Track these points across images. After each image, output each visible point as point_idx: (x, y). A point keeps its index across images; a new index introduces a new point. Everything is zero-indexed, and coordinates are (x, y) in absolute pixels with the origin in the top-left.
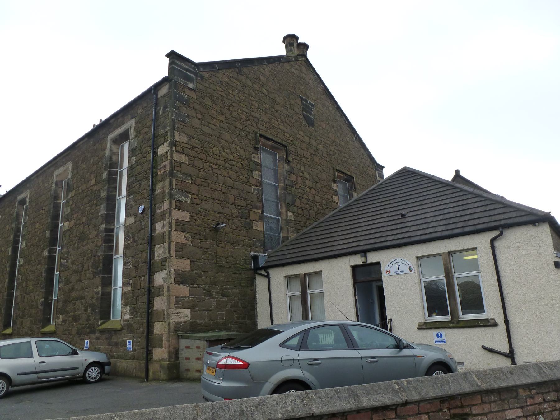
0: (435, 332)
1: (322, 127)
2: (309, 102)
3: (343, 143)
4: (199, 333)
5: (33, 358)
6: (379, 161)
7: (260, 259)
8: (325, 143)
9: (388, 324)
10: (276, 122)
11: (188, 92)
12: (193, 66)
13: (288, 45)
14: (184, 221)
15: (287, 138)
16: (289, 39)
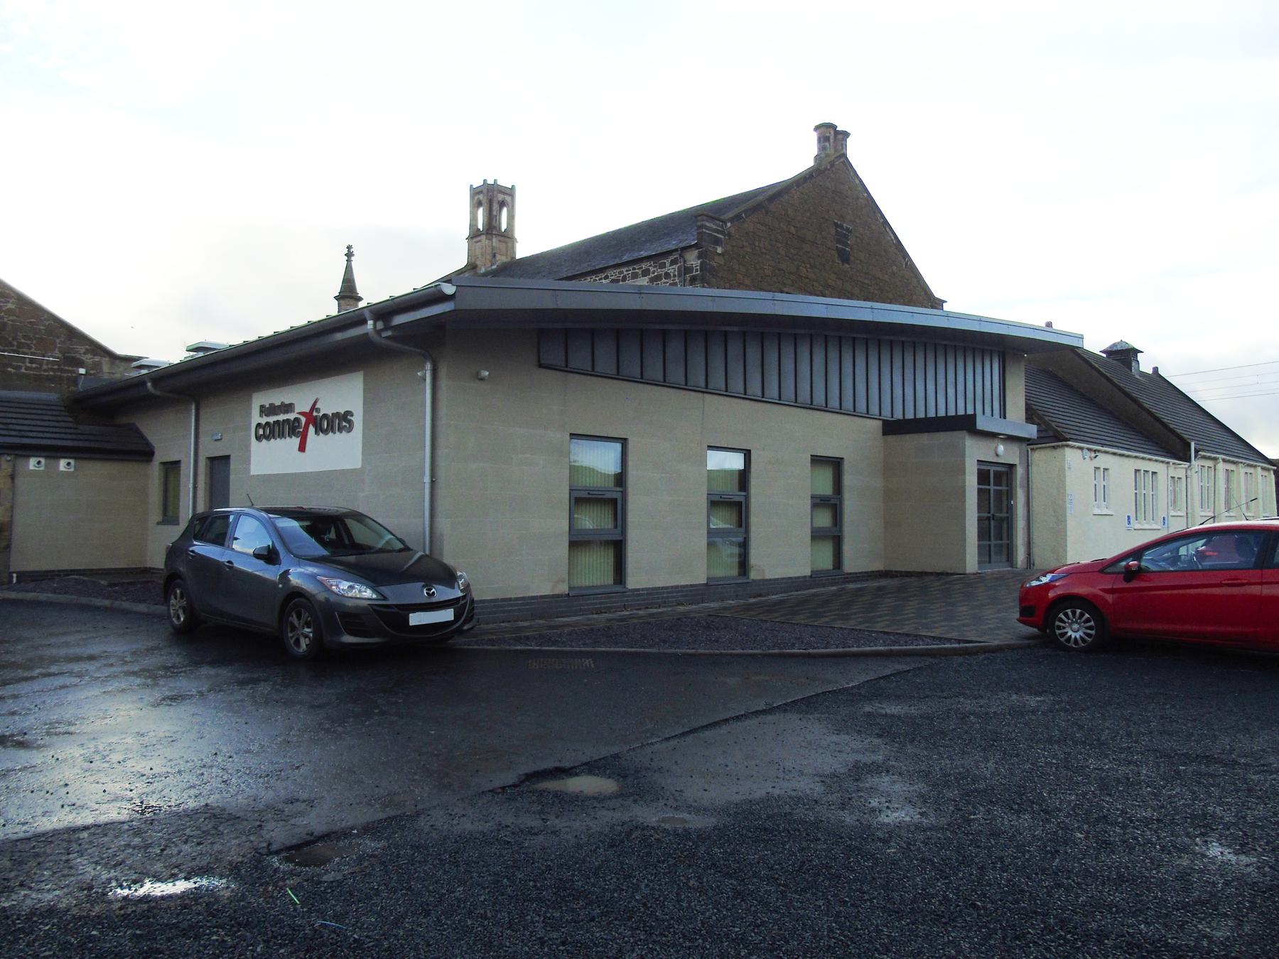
0: (434, 600)
1: (860, 260)
2: (847, 227)
3: (886, 278)
4: (1012, 521)
5: (814, 526)
6: (937, 295)
7: (845, 463)
8: (863, 283)
9: (42, 443)
10: (804, 270)
11: (717, 258)
12: (721, 223)
13: (822, 140)
14: (1162, 574)
15: (816, 288)
16: (823, 129)
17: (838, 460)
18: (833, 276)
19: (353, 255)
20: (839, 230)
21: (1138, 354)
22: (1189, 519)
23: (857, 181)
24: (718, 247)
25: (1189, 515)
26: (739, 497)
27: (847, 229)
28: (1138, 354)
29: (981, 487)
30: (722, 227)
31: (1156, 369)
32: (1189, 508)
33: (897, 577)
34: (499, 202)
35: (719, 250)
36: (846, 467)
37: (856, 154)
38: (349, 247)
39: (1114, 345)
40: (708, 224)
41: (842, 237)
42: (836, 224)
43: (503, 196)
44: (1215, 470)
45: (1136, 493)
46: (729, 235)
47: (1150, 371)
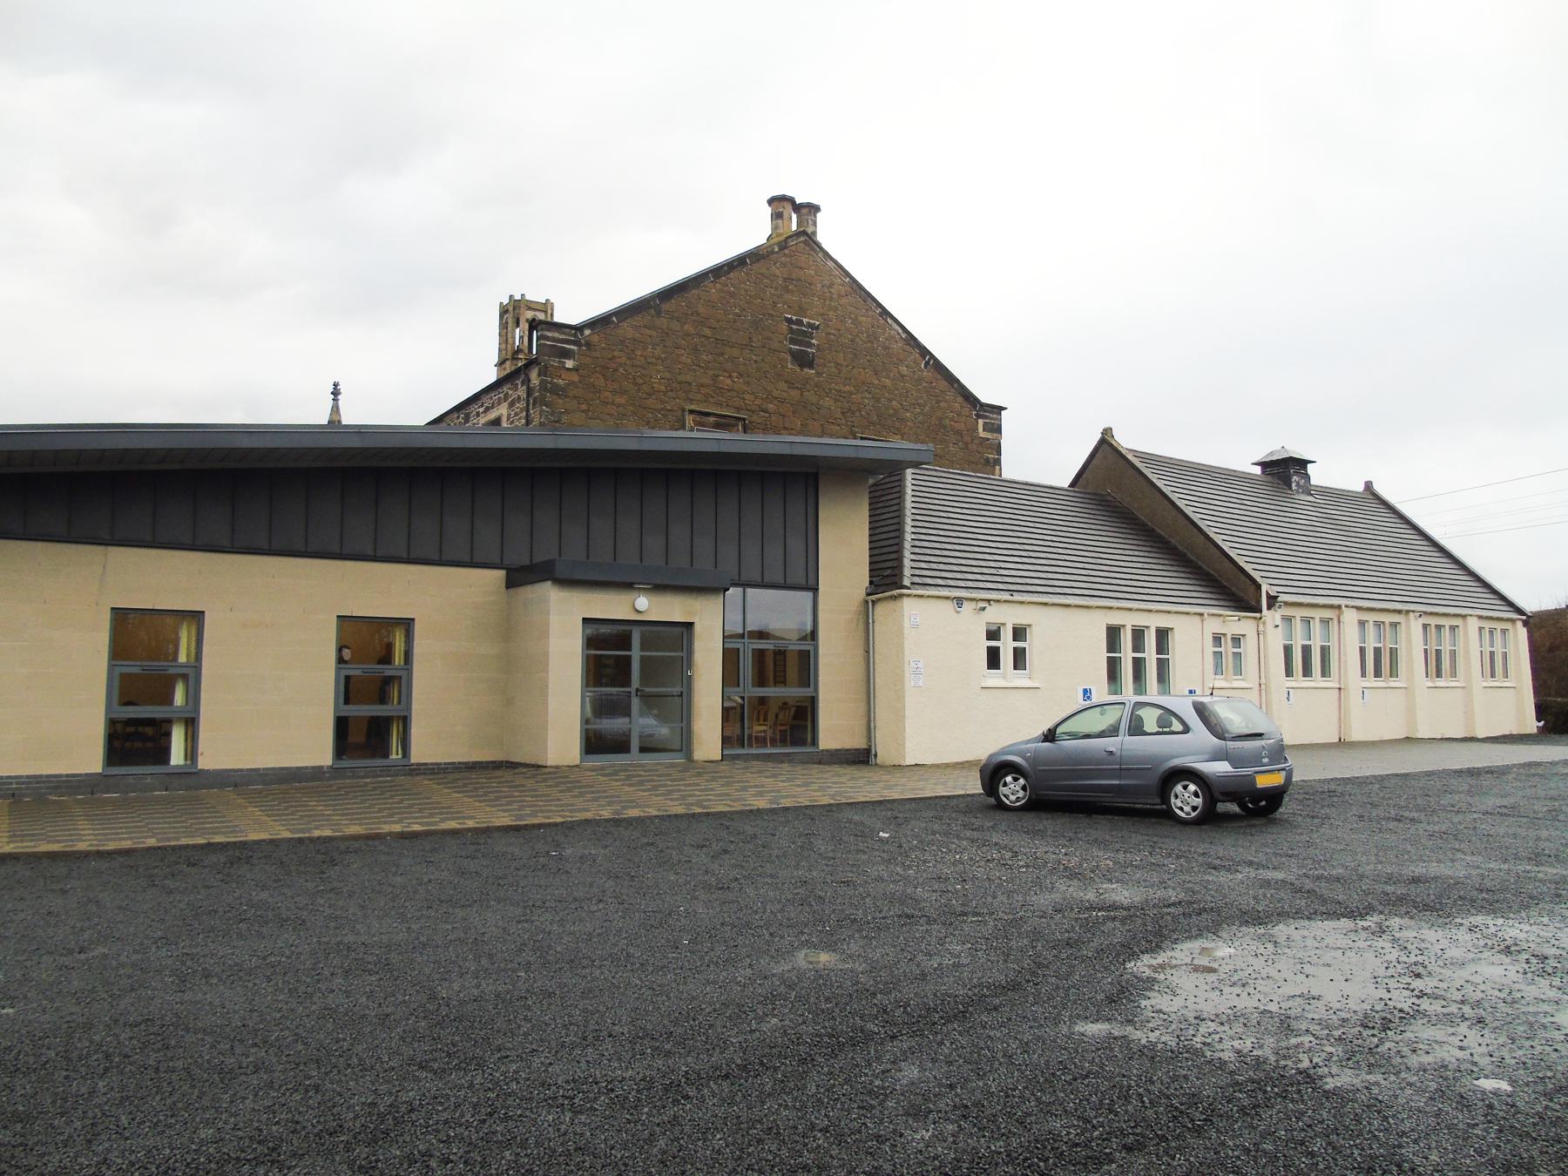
6: (985, 397)
17: (407, 621)
18: (783, 385)
19: (340, 394)
20: (794, 327)
21: (1309, 465)
22: (1263, 692)
23: (830, 264)
24: (567, 361)
25: (1263, 686)
26: (197, 664)
27: (810, 325)
28: (1309, 465)
29: (643, 653)
30: (575, 335)
31: (1369, 485)
32: (1263, 677)
33: (488, 767)
34: (527, 320)
35: (569, 364)
36: (418, 629)
37: (827, 234)
38: (336, 385)
39: (1271, 453)
40: (549, 334)
41: (800, 335)
42: (789, 321)
43: (534, 313)
44: (1339, 622)
45: (1482, 651)
46: (588, 344)
47: (1360, 488)
